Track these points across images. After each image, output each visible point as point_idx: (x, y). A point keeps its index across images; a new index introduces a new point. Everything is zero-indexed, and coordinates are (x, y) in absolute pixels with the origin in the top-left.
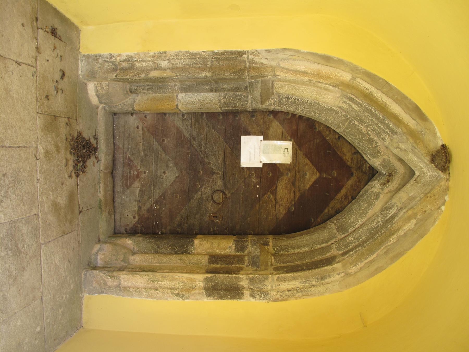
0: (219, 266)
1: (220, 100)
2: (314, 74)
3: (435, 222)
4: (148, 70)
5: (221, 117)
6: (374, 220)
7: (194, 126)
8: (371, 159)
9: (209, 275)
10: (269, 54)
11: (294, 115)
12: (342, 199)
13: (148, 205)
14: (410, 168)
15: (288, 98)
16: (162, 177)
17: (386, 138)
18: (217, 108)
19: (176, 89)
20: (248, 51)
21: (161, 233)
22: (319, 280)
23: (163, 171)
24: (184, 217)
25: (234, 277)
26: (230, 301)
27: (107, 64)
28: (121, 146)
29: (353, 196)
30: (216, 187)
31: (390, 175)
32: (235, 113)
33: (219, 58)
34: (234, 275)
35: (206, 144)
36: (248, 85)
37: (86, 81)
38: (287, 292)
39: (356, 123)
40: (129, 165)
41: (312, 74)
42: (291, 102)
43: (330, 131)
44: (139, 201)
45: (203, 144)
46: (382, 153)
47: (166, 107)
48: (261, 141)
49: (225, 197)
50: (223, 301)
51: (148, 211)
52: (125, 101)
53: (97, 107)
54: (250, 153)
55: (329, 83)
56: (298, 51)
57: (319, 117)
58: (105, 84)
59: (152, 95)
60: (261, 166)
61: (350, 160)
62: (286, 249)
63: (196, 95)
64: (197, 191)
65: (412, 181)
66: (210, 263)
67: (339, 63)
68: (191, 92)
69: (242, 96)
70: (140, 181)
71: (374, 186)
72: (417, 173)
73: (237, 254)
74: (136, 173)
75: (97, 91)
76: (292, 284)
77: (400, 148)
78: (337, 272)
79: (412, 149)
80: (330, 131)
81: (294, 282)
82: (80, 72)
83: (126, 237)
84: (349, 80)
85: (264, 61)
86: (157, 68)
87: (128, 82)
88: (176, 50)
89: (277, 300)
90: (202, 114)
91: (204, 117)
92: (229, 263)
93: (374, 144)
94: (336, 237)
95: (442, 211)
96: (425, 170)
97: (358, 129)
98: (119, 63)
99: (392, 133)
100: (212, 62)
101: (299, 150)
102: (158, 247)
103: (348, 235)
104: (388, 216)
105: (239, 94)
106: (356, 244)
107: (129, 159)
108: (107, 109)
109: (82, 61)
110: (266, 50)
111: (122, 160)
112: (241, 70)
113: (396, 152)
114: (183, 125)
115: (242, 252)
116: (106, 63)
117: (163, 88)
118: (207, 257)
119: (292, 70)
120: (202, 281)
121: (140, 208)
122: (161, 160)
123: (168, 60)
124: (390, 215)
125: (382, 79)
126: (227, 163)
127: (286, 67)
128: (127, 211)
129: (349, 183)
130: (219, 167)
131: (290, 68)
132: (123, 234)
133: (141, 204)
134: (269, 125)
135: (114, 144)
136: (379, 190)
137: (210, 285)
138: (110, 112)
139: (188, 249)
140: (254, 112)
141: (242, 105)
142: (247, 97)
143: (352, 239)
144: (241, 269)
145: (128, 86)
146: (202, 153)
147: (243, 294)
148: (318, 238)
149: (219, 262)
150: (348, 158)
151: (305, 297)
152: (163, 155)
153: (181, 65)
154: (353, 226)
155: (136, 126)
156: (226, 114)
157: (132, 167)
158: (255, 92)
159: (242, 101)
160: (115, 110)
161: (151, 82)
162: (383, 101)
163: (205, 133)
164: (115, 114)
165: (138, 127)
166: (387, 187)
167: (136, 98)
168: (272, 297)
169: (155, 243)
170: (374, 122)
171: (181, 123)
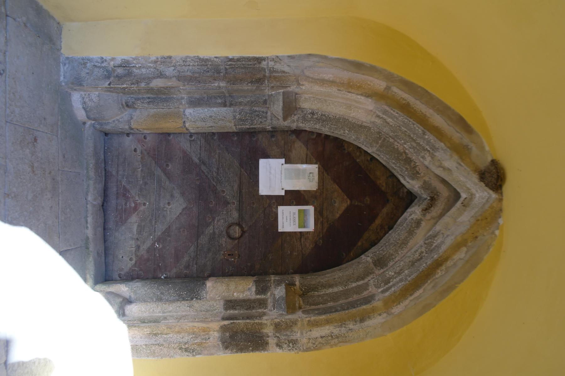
0: (236, 312)
1: (235, 117)
2: (343, 83)
3: (488, 249)
4: (149, 78)
5: (236, 138)
6: (417, 250)
7: (204, 149)
8: (410, 181)
9: (226, 322)
10: (292, 60)
11: (319, 135)
12: (377, 229)
13: (148, 244)
14: (455, 189)
15: (313, 114)
16: (165, 209)
17: (426, 156)
18: (231, 127)
19: (183, 103)
20: (267, 57)
21: (165, 277)
22: (358, 323)
23: (167, 202)
24: (192, 256)
25: (256, 323)
26: (251, 353)
27: (96, 70)
28: (114, 173)
29: (389, 226)
30: (231, 219)
31: (433, 199)
32: (252, 133)
33: (234, 65)
34: (256, 321)
35: (218, 169)
36: (267, 98)
37: (69, 91)
38: (320, 339)
39: (391, 140)
40: (124, 195)
41: (341, 83)
42: (317, 118)
43: (361, 152)
44: (137, 239)
45: (215, 169)
46: (422, 174)
47: (170, 125)
48: (282, 164)
49: (243, 232)
50: (243, 354)
51: (148, 251)
52: (120, 116)
53: (84, 123)
54: (270, 180)
55: (360, 93)
56: (325, 58)
57: (348, 134)
58: (94, 95)
59: (153, 110)
60: (283, 193)
61: (384, 184)
62: (315, 289)
63: (206, 110)
64: (208, 225)
65: (458, 204)
66: (226, 309)
67: (372, 70)
68: (200, 107)
69: (259, 111)
70: (138, 214)
71: (414, 212)
72: (464, 195)
73: (258, 297)
74: (133, 205)
75: (85, 103)
76: (325, 330)
77: (442, 167)
78: (379, 313)
79: (457, 167)
80: (361, 152)
81: (327, 327)
82: (62, 78)
83: (120, 283)
84: (383, 90)
85: (286, 69)
86: (161, 75)
87: (124, 94)
88: (184, 54)
89: (308, 350)
90: (213, 134)
91: (215, 138)
92: (249, 308)
93: (412, 164)
94: (373, 273)
95: (496, 236)
96: (473, 191)
97: (394, 148)
98: (112, 69)
99: (433, 150)
100: (226, 69)
101: (326, 175)
102: (162, 293)
103: (387, 270)
104: (432, 245)
105: (257, 109)
106: (398, 279)
107: (125, 189)
108: (98, 127)
109: (65, 65)
110: (289, 56)
111: (115, 189)
112: (260, 79)
113: (439, 172)
114: (191, 147)
115: (264, 295)
116: (96, 69)
117: (167, 101)
118: (222, 303)
119: (318, 79)
120: (217, 331)
121: (138, 247)
122: (164, 189)
123: (173, 66)
124: (434, 245)
125: (420, 87)
126: (243, 191)
127: (311, 75)
128: (121, 252)
129: (385, 210)
130: (234, 196)
131: (316, 77)
132: (116, 280)
133: (139, 243)
134: (291, 146)
135: (105, 170)
136: (420, 216)
137: (227, 334)
138: (101, 131)
139: (198, 294)
140: (274, 132)
141: (261, 122)
142: (267, 113)
143: (393, 274)
144: (264, 314)
145: (125, 98)
146: (213, 180)
147: (267, 343)
148: (353, 274)
149: (237, 307)
150: (382, 182)
151: (342, 344)
152: (167, 183)
153: (189, 74)
154: (393, 259)
155: (133, 149)
156: (241, 134)
157: (128, 198)
158: (275, 106)
159: (261, 118)
160: (108, 128)
161: (152, 94)
162: (422, 113)
163: (217, 156)
164: (106, 134)
165: (135, 150)
166: (429, 213)
167: (133, 114)
168: (303, 345)
169: (158, 289)
170: (412, 138)
171: (188, 145)
